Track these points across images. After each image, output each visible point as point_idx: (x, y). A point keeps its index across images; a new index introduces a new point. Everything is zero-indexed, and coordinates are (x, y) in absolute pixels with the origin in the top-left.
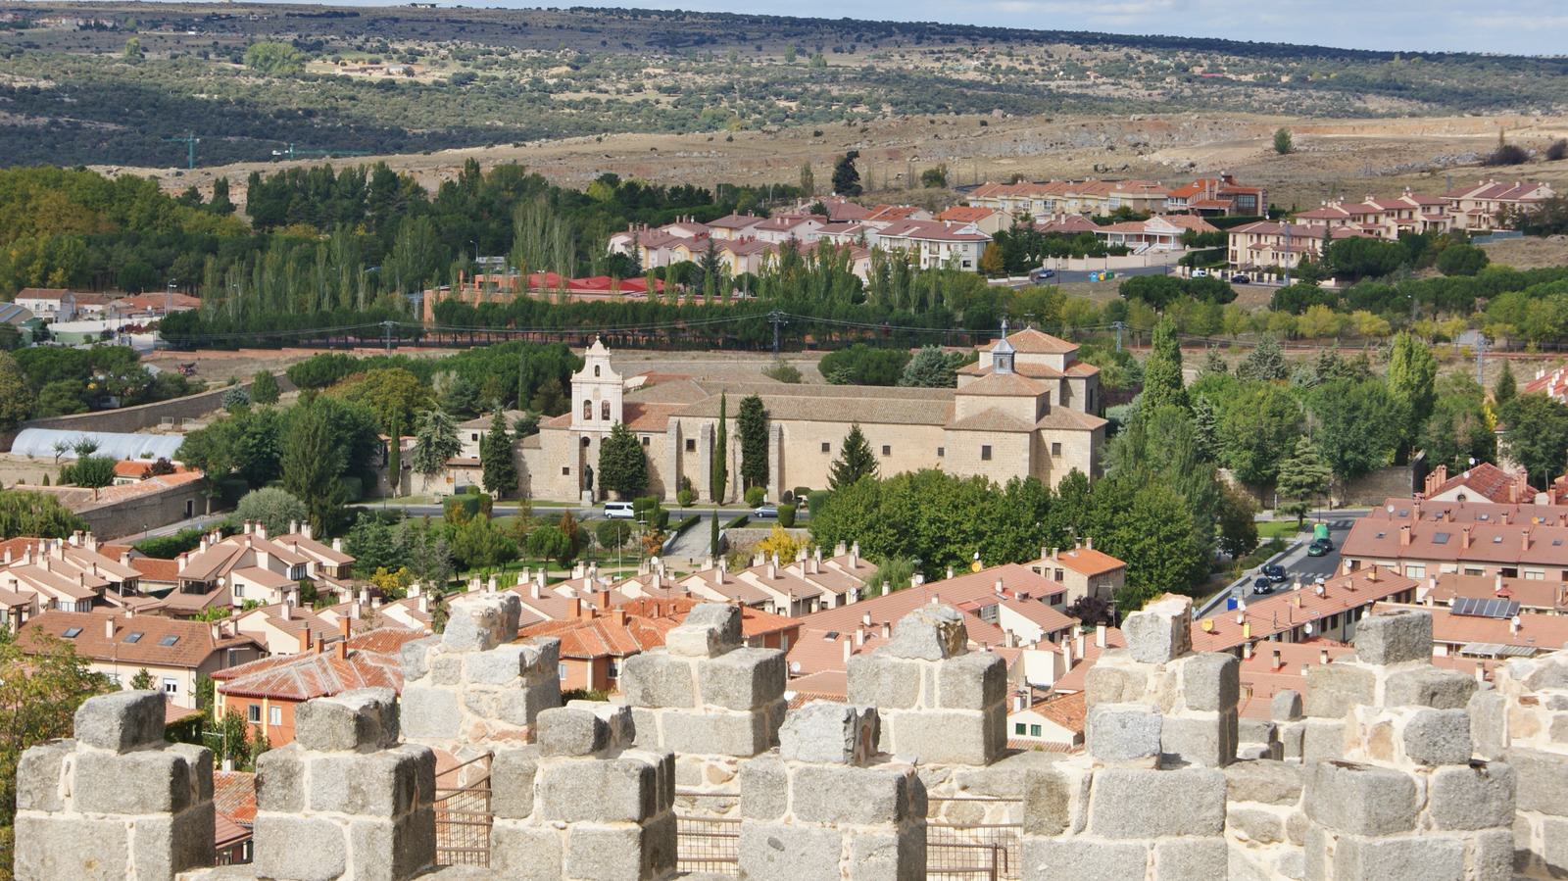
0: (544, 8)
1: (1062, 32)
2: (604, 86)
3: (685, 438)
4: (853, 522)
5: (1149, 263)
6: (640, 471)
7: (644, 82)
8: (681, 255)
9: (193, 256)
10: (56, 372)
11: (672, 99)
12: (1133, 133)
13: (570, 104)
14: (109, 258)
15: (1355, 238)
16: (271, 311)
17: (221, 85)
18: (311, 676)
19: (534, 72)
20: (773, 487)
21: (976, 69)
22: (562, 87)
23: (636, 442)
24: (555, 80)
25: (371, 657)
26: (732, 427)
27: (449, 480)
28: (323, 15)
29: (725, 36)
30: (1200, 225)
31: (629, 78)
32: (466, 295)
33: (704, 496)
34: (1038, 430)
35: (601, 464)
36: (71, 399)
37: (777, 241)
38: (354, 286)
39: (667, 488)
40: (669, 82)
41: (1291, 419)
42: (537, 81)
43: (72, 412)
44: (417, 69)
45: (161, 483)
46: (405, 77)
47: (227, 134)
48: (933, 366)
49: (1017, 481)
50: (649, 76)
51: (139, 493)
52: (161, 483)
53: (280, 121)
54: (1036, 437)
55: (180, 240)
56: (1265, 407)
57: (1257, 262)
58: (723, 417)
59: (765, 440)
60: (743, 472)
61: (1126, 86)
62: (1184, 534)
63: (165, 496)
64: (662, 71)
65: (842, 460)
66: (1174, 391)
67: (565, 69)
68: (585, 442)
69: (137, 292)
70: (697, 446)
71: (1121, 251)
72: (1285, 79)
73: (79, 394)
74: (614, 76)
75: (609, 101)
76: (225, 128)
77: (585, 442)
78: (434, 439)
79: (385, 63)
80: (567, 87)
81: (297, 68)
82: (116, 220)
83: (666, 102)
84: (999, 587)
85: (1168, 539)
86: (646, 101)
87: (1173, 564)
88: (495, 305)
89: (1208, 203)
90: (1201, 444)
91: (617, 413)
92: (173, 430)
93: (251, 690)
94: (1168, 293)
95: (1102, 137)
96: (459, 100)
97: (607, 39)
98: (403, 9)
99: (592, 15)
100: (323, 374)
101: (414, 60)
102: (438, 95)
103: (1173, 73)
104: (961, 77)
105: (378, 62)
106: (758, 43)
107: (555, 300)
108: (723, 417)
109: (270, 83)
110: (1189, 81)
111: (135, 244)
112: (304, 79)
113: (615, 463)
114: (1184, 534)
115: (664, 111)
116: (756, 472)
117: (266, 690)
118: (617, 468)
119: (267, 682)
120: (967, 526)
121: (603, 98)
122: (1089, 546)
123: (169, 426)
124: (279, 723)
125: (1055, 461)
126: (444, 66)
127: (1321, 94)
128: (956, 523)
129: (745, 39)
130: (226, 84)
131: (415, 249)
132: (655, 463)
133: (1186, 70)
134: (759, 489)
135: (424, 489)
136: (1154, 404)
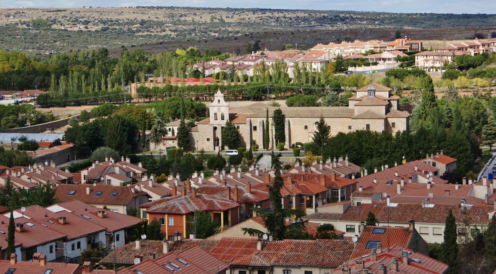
0: (128, 7)
2: (152, 30)
3: (253, 126)
4: (340, 149)
5: (386, 68)
6: (237, 138)
7: (166, 28)
8: (217, 70)
9: (41, 77)
10: (6, 113)
11: (176, 34)
12: (344, 35)
13: (142, 36)
14: (10, 79)
16: (76, 93)
17: (24, 33)
18: (184, 204)
19: (128, 26)
20: (287, 143)
22: (138, 31)
23: (235, 128)
25: (207, 196)
26: (271, 121)
27: (164, 144)
28: (54, 11)
29: (189, 14)
30: (402, 55)
31: (160, 27)
32: (147, 85)
33: (261, 147)
34: (386, 118)
35: (222, 136)
36: (13, 123)
37: (61, 137)
38: (106, 83)
39: (247, 145)
40: (174, 28)
41: (482, 110)
43: (13, 127)
44: (89, 27)
45: (57, 149)
46: (85, 29)
47: (28, 49)
48: (334, 99)
50: (167, 27)
51: (50, 152)
52: (57, 149)
53: (45, 44)
54: (386, 120)
55: (35, 72)
56: (472, 107)
57: (426, 65)
58: (268, 117)
59: (284, 125)
60: (275, 138)
61: (325, 26)
62: (467, 150)
63: (60, 153)
64: (171, 25)
65: (317, 131)
66: (432, 103)
68: (215, 129)
69: (23, 90)
70: (258, 128)
71: (376, 64)
72: (376, 22)
73: (15, 121)
74: (155, 27)
75: (155, 35)
76: (27, 47)
77: (215, 129)
78: (158, 129)
79: (78, 25)
80: (140, 31)
81: (49, 27)
82: (11, 67)
83: (173, 35)
84: (416, 169)
85: (461, 152)
86: (167, 35)
87: (464, 162)
88: (158, 88)
89: (401, 47)
90: (447, 121)
91: (227, 117)
92: (51, 133)
93: (160, 211)
94: (403, 75)
95: (334, 37)
96: (105, 36)
97: (150, 16)
100: (104, 111)
101: (87, 24)
102: (98, 34)
105: (76, 25)
106: (201, 16)
107: (180, 85)
108: (268, 117)
109: (41, 32)
111: (19, 74)
112: (52, 30)
113: (228, 135)
114: (467, 150)
115: (173, 38)
116: (280, 137)
117: (166, 211)
118: (229, 137)
119: (166, 208)
120: (381, 150)
121: (153, 34)
122: (442, 153)
123: (50, 131)
124: (173, 225)
125: (393, 129)
126: (98, 25)
128: (377, 149)
129: (196, 15)
130: (26, 33)
131: (124, 71)
132: (242, 136)
134: (282, 144)
135: (155, 148)
136: (425, 108)
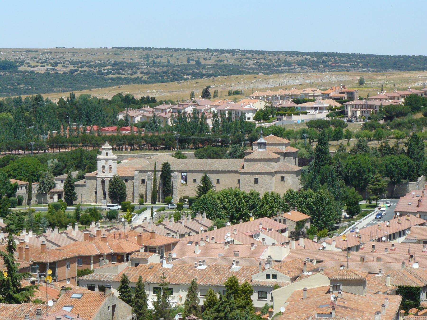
1: (283, 51)
2: (123, 72)
11: (147, 76)
15: (391, 105)
21: (253, 64)
22: (108, 73)
24: (106, 71)
31: (132, 69)
42: (100, 71)
49: (268, 193)
67: (110, 67)
77: (103, 182)
86: (138, 77)
98: (53, 49)
99: (119, 49)
101: (56, 66)
103: (321, 64)
104: (249, 67)
110: (327, 66)
112: (17, 73)
127: (373, 69)
133: (326, 62)
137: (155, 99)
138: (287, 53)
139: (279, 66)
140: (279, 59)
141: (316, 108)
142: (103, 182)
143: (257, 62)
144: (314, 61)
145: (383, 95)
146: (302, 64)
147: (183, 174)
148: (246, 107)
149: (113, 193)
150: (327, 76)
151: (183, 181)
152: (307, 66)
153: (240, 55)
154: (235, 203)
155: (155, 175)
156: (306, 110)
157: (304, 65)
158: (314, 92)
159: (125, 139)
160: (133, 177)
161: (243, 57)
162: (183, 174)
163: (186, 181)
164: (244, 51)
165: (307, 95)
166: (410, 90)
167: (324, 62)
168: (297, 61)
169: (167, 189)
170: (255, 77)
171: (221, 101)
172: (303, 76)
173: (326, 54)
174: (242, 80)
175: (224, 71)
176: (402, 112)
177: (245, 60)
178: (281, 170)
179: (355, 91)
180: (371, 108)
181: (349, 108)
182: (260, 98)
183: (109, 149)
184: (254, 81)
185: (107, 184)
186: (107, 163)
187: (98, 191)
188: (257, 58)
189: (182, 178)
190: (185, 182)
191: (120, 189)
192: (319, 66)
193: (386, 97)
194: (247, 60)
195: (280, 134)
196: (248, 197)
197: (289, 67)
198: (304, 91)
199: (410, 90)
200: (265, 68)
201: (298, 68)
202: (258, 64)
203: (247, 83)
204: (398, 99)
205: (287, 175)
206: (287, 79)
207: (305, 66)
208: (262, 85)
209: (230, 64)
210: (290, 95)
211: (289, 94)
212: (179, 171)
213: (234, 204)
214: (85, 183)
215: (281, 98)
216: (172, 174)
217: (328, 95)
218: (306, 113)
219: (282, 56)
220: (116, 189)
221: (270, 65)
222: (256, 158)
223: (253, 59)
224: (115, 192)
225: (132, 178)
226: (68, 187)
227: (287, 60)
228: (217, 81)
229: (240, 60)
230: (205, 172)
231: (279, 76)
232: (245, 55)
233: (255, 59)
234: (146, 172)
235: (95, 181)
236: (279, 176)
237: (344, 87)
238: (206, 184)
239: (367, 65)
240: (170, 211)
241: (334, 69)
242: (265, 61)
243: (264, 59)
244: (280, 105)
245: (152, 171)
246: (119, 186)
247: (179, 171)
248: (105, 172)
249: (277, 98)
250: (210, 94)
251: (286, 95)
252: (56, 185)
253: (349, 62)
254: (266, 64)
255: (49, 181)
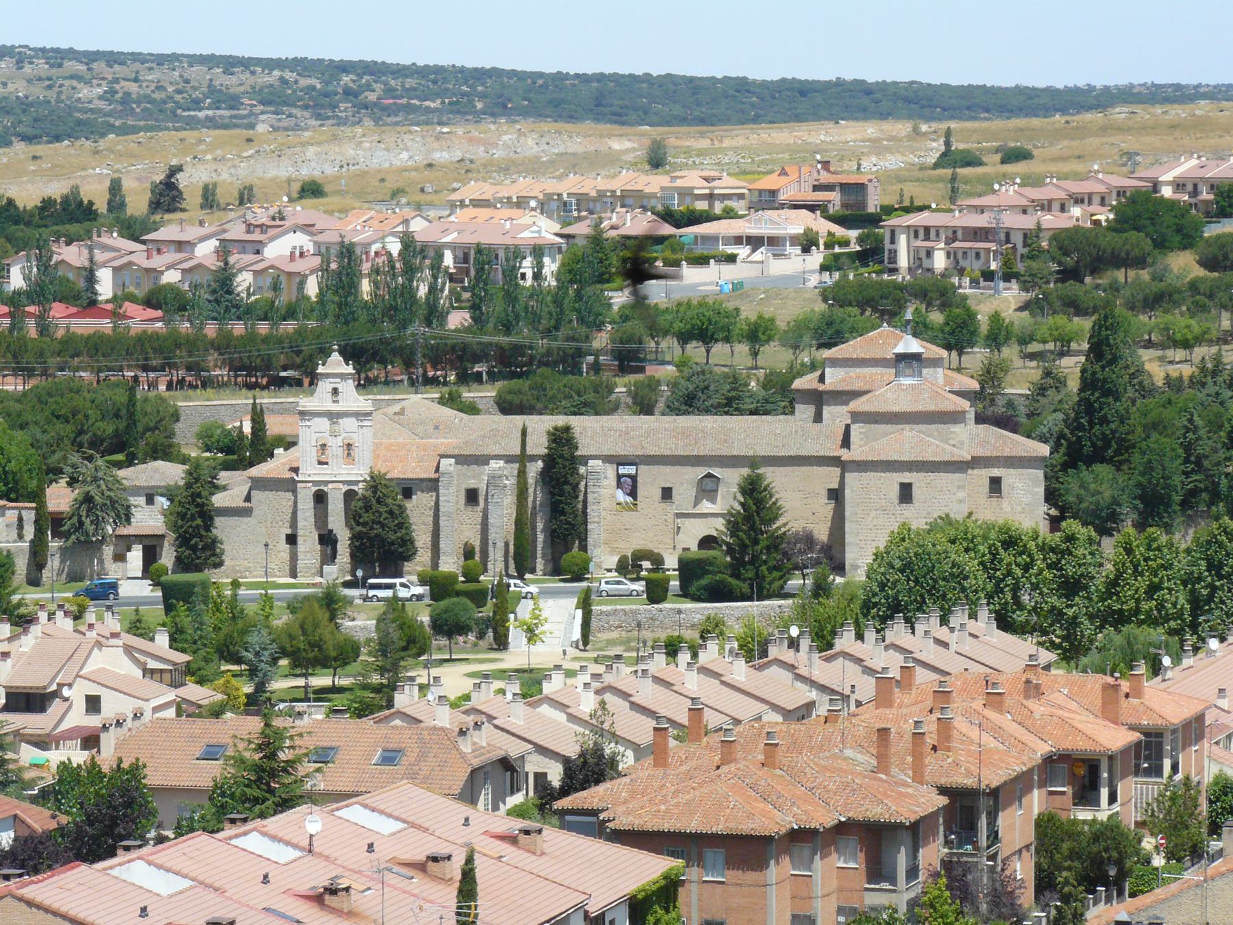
77: (320, 498)
137: (94, 208)
138: (209, 61)
139: (195, 106)
140: (187, 81)
141: (755, 242)
142: (320, 498)
143: (113, 92)
144: (314, 88)
145: (1011, 193)
146: (274, 99)
147: (622, 470)
148: (526, 234)
149: (369, 538)
150: (506, 138)
151: (621, 496)
152: (295, 106)
153: (42, 66)
154: (1009, 573)
155: (522, 473)
156: (721, 247)
157: (285, 103)
158: (712, 185)
159: (147, 345)
160: (437, 480)
161: (55, 72)
162: (622, 470)
163: (633, 493)
164: (57, 51)
165: (685, 193)
166: (1100, 176)
167: (348, 92)
168: (253, 87)
169: (569, 523)
170: (249, 140)
171: (372, 213)
172: (423, 137)
173: (344, 67)
174: (203, 147)
175: (20, 122)
176: (1123, 254)
177: (67, 83)
178: (988, 454)
179: (870, 181)
180: (987, 240)
181: (902, 240)
182: (533, 204)
183: (343, 376)
184: (251, 152)
185: (336, 506)
186: (336, 427)
187: (300, 532)
188: (110, 77)
189: (619, 485)
190: (629, 499)
191: (397, 525)
192: (338, 107)
193: (1024, 202)
194: (75, 83)
195: (722, 329)
196: (1053, 550)
197: (232, 108)
198: (674, 178)
199: (1100, 176)
200: (145, 110)
201: (262, 113)
202: (118, 96)
203: (223, 159)
204: (1063, 208)
205: (1012, 471)
206: (367, 145)
207: (288, 105)
208: (278, 166)
209: (18, 98)
210: (618, 193)
211: (614, 192)
212: (607, 459)
213: (1005, 576)
214: (247, 504)
215: (578, 205)
216: (582, 470)
217: (773, 193)
218: (732, 259)
219: (197, 73)
220: (383, 526)
221: (164, 102)
222: (896, 409)
223: (94, 81)
224: (377, 536)
225: (432, 485)
226: (193, 518)
227: (216, 83)
228: (111, 151)
229: (47, 83)
230: (753, 462)
231: (335, 137)
232: (60, 66)
233: (103, 79)
234: (482, 460)
235: (289, 495)
236: (981, 476)
237: (826, 164)
238: (759, 502)
239: (505, 107)
240: (611, 603)
241: (393, 119)
242: (140, 87)
243: (136, 80)
244: (613, 228)
245: (509, 459)
246: (391, 513)
247: (607, 459)
248: (326, 463)
249: (565, 204)
250: (181, 193)
251: (601, 194)
252: (133, 510)
253: (438, 95)
254: (141, 100)
255: (112, 494)
